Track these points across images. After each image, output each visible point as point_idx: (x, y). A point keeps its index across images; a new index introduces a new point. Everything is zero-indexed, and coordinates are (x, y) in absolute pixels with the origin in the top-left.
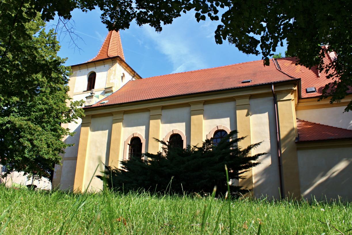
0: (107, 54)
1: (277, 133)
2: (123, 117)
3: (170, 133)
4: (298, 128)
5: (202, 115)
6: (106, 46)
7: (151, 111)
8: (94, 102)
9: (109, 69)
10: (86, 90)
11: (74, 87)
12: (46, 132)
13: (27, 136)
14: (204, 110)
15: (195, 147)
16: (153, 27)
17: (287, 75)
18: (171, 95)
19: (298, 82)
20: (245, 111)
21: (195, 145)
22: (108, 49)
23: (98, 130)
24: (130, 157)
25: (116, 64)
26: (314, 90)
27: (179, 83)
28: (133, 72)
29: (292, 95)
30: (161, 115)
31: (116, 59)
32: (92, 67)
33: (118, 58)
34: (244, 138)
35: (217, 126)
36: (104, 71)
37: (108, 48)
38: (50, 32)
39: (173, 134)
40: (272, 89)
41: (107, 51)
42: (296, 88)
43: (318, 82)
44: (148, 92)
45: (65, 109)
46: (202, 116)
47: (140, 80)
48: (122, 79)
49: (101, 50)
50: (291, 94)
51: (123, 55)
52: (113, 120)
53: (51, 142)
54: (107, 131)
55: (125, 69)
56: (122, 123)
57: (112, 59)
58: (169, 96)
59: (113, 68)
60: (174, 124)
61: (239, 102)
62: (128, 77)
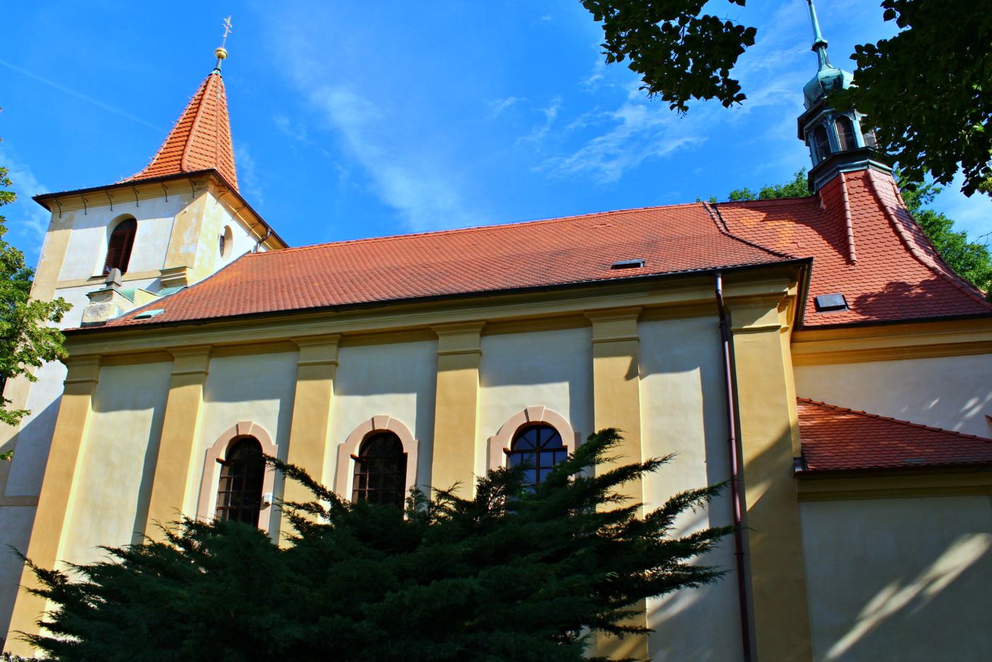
0: (180, 165)
1: (730, 439)
4: (802, 423)
5: (477, 371)
6: (181, 139)
7: (302, 350)
8: (114, 311)
9: (179, 212)
14: (483, 352)
17: (761, 249)
18: (373, 299)
19: (804, 269)
20: (624, 363)
21: (445, 489)
22: (183, 150)
24: (222, 505)
25: (204, 196)
26: (840, 302)
28: (261, 227)
29: (781, 313)
30: (336, 364)
31: (204, 179)
32: (124, 201)
33: (212, 177)
34: (659, 463)
35: (526, 411)
37: (185, 146)
40: (717, 291)
41: (182, 155)
42: (793, 291)
43: (851, 279)
44: (301, 289)
46: (474, 373)
47: (281, 251)
49: (162, 151)
50: (780, 311)
52: (173, 375)
54: (151, 411)
55: (234, 215)
56: (201, 387)
57: (193, 180)
58: (365, 300)
59: (192, 208)
60: (377, 399)
61: (604, 330)
62: (244, 242)
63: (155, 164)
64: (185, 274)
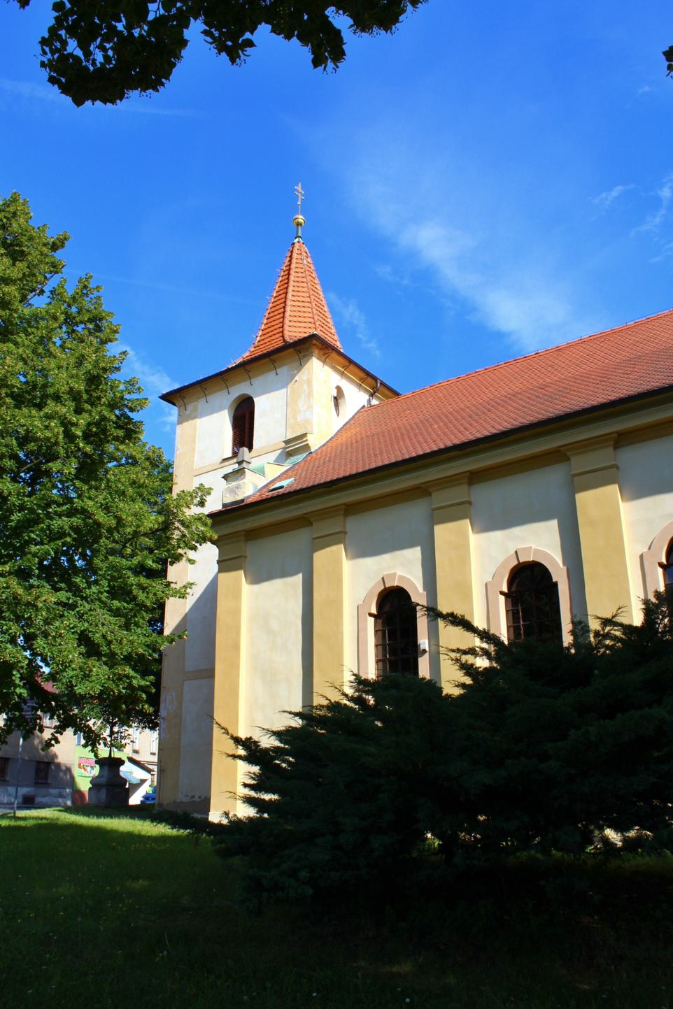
0: (283, 336)
2: (345, 527)
3: (506, 561)
7: (433, 494)
8: (250, 488)
10: (230, 455)
11: (194, 449)
12: (86, 604)
13: (10, 629)
15: (606, 622)
16: (295, 39)
21: (609, 616)
23: (269, 577)
27: (520, 389)
30: (470, 503)
31: (307, 345)
32: (239, 382)
33: (314, 342)
36: (278, 389)
37: (283, 317)
38: (81, 286)
39: (519, 564)
41: (283, 327)
44: (421, 434)
45: (140, 523)
47: (394, 400)
48: (337, 406)
51: (333, 331)
52: (314, 539)
53: (104, 636)
55: (342, 374)
59: (302, 376)
60: (517, 531)
62: (357, 398)
63: (259, 341)
64: (307, 440)
